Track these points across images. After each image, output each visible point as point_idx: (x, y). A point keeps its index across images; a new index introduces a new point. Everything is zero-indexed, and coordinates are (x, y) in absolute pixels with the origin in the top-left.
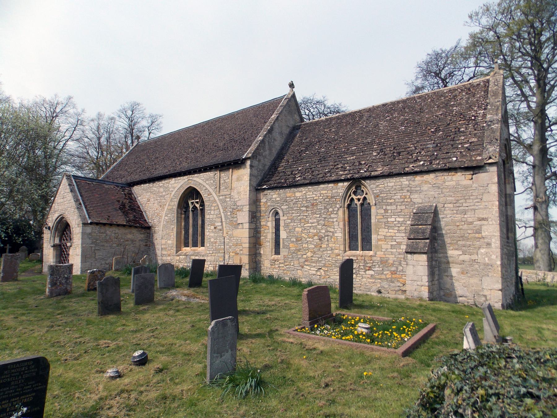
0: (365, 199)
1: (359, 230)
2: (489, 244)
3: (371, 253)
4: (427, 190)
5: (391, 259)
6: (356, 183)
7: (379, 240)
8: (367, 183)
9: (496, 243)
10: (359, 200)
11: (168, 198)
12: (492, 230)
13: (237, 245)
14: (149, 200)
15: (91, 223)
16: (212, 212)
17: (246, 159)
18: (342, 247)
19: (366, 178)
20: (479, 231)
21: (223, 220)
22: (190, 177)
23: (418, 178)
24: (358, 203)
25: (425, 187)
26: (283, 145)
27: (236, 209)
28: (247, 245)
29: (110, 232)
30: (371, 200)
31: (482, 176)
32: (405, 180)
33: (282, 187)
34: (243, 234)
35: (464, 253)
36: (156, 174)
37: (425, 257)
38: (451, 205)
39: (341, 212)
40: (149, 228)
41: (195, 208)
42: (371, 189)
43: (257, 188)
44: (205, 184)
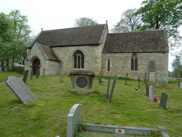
3: (137, 71)
6: (134, 53)
8: (137, 53)
11: (69, 53)
13: (97, 68)
15: (49, 60)
19: (137, 52)
21: (92, 61)
22: (79, 47)
23: (151, 54)
25: (152, 56)
30: (138, 58)
32: (147, 54)
33: (111, 53)
35: (161, 71)
41: (79, 57)
44: (84, 49)
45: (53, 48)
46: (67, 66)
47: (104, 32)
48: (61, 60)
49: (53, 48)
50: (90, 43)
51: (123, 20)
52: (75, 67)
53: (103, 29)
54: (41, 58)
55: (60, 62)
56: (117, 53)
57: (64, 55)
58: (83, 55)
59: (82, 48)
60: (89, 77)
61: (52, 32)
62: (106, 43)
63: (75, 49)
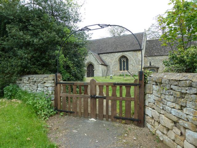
22: (123, 53)
45: (100, 55)
46: (113, 69)
47: (144, 39)
48: (107, 64)
49: (100, 55)
50: (133, 49)
51: (153, 24)
52: (121, 70)
53: (143, 37)
54: (95, 63)
55: (107, 66)
56: (158, 56)
57: (111, 60)
58: (127, 60)
59: (126, 54)
60: (156, 69)
61: (96, 41)
62: (146, 49)
63: (120, 54)
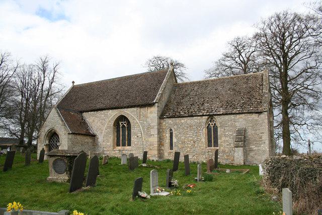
0: (215, 124)
1: (213, 138)
2: (265, 143)
4: (241, 121)
5: (227, 150)
6: (211, 117)
7: (221, 142)
8: (216, 117)
9: (267, 142)
10: (212, 124)
11: (107, 120)
12: (266, 137)
14: (94, 121)
16: (136, 129)
17: (156, 103)
18: (205, 146)
19: (215, 115)
20: (261, 138)
23: (238, 116)
24: (212, 126)
25: (241, 120)
26: (159, 90)
27: (149, 127)
28: (157, 145)
29: (79, 137)
30: (218, 125)
31: (262, 116)
32: (232, 117)
34: (154, 139)
36: (98, 107)
37: (242, 149)
38: (251, 128)
39: (204, 130)
40: (93, 136)
42: (218, 120)
43: (161, 117)
